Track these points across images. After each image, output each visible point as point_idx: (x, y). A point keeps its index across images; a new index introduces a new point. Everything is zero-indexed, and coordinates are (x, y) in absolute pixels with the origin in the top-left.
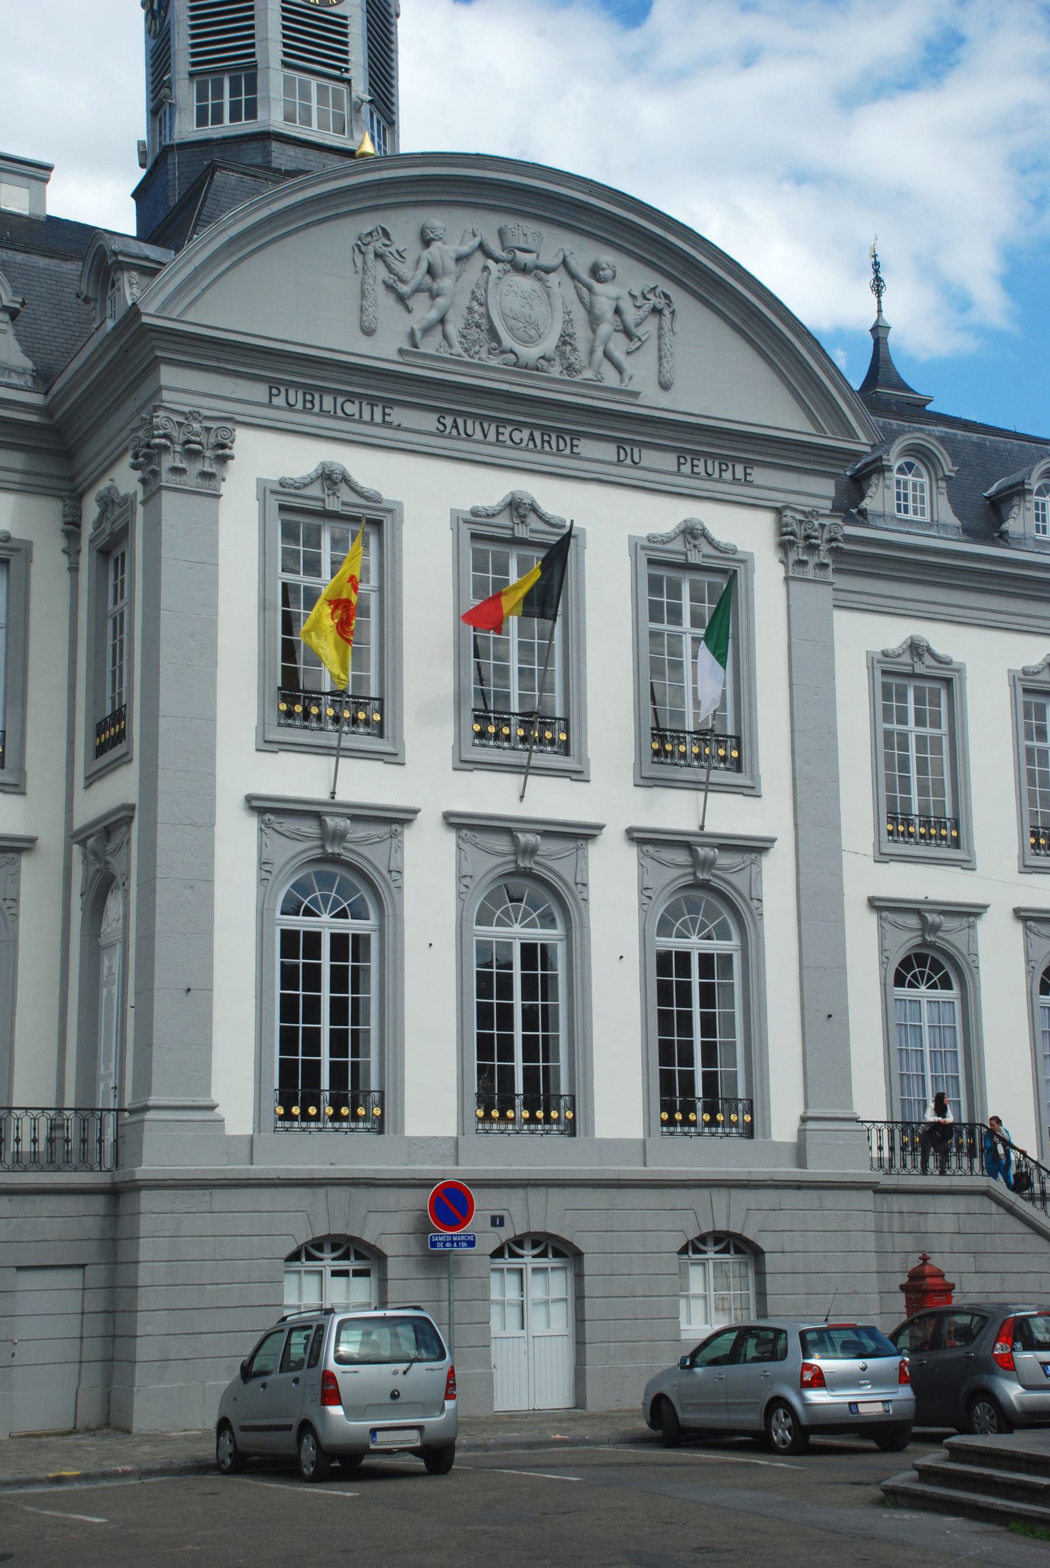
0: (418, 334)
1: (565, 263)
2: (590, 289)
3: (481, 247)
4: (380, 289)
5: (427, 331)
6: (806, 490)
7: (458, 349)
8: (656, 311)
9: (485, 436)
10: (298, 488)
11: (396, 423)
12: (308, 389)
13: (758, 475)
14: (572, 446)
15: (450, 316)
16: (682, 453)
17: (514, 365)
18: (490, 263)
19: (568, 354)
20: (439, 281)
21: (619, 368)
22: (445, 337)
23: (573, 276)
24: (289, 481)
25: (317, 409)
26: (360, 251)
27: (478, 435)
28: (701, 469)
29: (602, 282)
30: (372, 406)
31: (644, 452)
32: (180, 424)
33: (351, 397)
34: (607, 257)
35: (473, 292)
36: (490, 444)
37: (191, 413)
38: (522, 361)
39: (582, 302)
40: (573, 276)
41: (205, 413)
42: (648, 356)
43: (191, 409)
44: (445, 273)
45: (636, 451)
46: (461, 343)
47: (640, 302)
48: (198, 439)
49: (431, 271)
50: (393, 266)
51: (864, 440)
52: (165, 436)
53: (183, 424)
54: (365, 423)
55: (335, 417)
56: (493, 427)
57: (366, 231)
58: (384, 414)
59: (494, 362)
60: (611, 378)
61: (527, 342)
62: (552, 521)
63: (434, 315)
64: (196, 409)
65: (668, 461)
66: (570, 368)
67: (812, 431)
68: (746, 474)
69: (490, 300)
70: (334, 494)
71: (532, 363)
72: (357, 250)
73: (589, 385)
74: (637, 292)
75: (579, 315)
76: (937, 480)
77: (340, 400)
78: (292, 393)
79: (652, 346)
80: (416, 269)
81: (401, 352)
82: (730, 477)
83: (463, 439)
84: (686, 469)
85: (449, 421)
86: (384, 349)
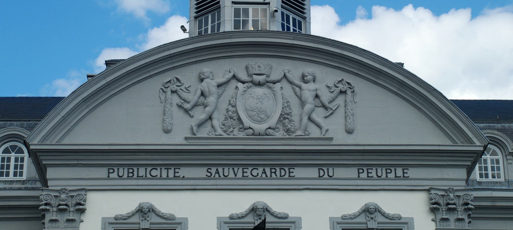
0: (195, 128)
1: (285, 76)
2: (300, 88)
3: (234, 77)
4: (175, 109)
5: (200, 125)
6: (446, 177)
7: (220, 131)
8: (341, 92)
9: (236, 175)
10: (125, 219)
11: (182, 176)
12: (130, 166)
13: (412, 173)
14: (290, 172)
15: (215, 116)
16: (360, 167)
17: (253, 135)
18: (240, 85)
19: (287, 124)
20: (207, 98)
21: (319, 127)
22: (213, 127)
23: (291, 83)
24: (119, 217)
25: (135, 176)
26: (163, 91)
27: (232, 175)
28: (373, 174)
29: (306, 83)
30: (168, 169)
31: (335, 169)
32: (56, 197)
33: (155, 167)
34: (310, 69)
35: (230, 101)
36: (239, 179)
37: (61, 190)
38: (257, 132)
39: (296, 95)
40: (291, 83)
41: (455, 188)
42: (339, 118)
43: (61, 188)
44: (210, 94)
45: (331, 170)
46: (222, 128)
47: (334, 88)
48: (453, 202)
49: (202, 94)
50: (182, 96)
51: (478, 143)
52: (46, 204)
53: (444, 195)
54: (164, 179)
55: (146, 178)
56: (241, 170)
57: (166, 81)
58: (175, 172)
59: (241, 135)
60: (315, 132)
61: (259, 122)
62: (279, 216)
63: (203, 116)
64: (64, 187)
65: (353, 172)
66: (288, 131)
67: (449, 143)
68: (404, 173)
69: (238, 104)
70: (145, 219)
71: (263, 132)
72: (161, 91)
73: (299, 139)
74: (331, 84)
75: (294, 102)
76: (506, 156)
77: (149, 169)
78: (121, 170)
79: (341, 112)
80: (195, 95)
81: (186, 139)
82: (394, 176)
83: (222, 179)
84: (364, 175)
85: (213, 170)
86: (177, 139)
